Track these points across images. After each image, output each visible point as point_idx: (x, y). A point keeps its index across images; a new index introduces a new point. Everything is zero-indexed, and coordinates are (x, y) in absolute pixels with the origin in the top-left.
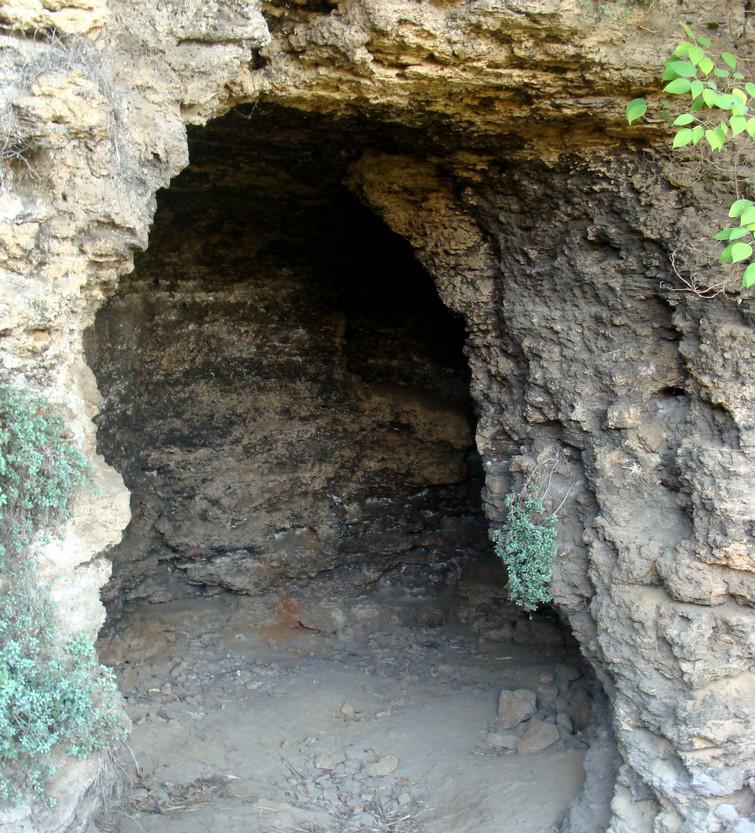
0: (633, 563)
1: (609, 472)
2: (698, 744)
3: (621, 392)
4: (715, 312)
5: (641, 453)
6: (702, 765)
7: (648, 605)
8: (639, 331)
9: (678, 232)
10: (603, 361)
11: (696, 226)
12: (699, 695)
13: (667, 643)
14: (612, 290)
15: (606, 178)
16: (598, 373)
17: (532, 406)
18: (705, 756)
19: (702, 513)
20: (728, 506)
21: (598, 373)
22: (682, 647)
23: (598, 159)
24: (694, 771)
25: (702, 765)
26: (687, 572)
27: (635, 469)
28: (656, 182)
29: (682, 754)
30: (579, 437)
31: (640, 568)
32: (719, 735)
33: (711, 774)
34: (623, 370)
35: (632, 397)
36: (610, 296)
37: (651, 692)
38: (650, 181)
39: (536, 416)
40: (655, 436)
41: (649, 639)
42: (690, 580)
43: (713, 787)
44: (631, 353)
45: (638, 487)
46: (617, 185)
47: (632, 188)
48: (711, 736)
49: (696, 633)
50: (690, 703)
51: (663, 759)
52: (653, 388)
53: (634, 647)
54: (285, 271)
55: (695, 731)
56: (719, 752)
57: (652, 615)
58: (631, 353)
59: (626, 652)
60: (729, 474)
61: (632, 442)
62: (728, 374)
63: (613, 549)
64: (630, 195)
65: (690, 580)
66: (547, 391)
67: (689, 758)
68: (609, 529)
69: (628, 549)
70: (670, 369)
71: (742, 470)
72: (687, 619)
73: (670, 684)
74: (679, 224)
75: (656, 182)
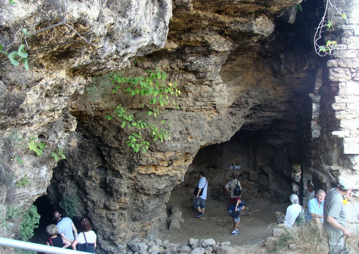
0: (99, 204)
1: (88, 186)
2: (118, 239)
3: (90, 168)
4: (113, 151)
5: (95, 181)
6: (120, 243)
7: (104, 212)
8: (92, 154)
9: (104, 135)
10: (84, 161)
11: (108, 134)
12: (117, 229)
13: (110, 220)
14: (86, 146)
15: (87, 124)
16: (83, 164)
17: (65, 172)
18: (120, 241)
19: (115, 192)
20: (122, 190)
21: (83, 164)
22: (114, 220)
23: (86, 120)
24: (119, 245)
25: (120, 243)
26: (113, 204)
27: (94, 184)
28: (98, 124)
29: (115, 242)
30: (78, 178)
31: (102, 205)
32: (123, 236)
33: (122, 245)
34: (89, 164)
35: (92, 169)
36: (86, 147)
37: (106, 231)
38: (96, 124)
39: (66, 175)
40: (99, 177)
41: (106, 220)
42: (114, 206)
43: (122, 247)
44: (91, 159)
45: (95, 188)
46: (89, 125)
47: (92, 125)
48: (121, 237)
49: (116, 217)
50: (115, 231)
51: (109, 245)
52: (96, 167)
53: (102, 222)
54: (313, 152)
55: (117, 236)
56: (123, 240)
57: (105, 215)
58: (91, 159)
59: (100, 223)
60: (120, 184)
61: (94, 179)
62: (118, 164)
63: (93, 202)
64: (91, 127)
65: (114, 206)
66: (69, 168)
67: (117, 242)
68: (91, 198)
69: (97, 201)
70: (100, 163)
71: (123, 183)
72: (113, 214)
73: (109, 228)
74: (104, 134)
75: (98, 124)
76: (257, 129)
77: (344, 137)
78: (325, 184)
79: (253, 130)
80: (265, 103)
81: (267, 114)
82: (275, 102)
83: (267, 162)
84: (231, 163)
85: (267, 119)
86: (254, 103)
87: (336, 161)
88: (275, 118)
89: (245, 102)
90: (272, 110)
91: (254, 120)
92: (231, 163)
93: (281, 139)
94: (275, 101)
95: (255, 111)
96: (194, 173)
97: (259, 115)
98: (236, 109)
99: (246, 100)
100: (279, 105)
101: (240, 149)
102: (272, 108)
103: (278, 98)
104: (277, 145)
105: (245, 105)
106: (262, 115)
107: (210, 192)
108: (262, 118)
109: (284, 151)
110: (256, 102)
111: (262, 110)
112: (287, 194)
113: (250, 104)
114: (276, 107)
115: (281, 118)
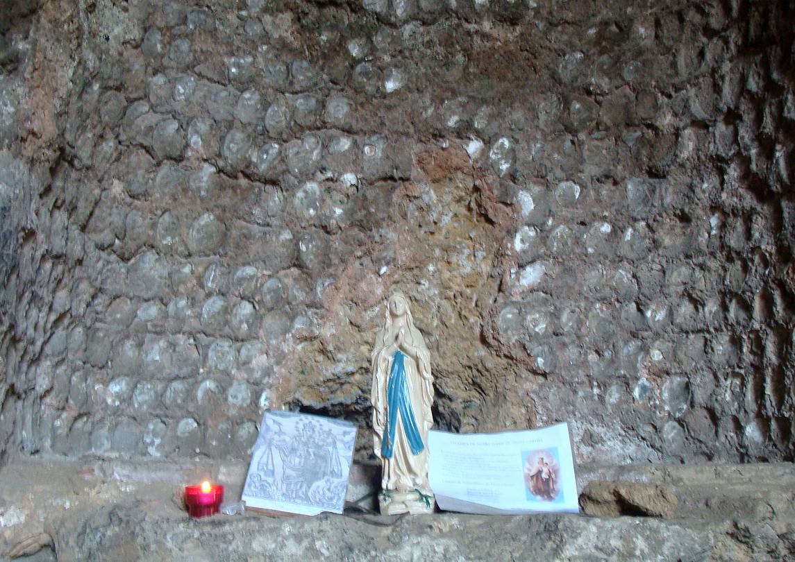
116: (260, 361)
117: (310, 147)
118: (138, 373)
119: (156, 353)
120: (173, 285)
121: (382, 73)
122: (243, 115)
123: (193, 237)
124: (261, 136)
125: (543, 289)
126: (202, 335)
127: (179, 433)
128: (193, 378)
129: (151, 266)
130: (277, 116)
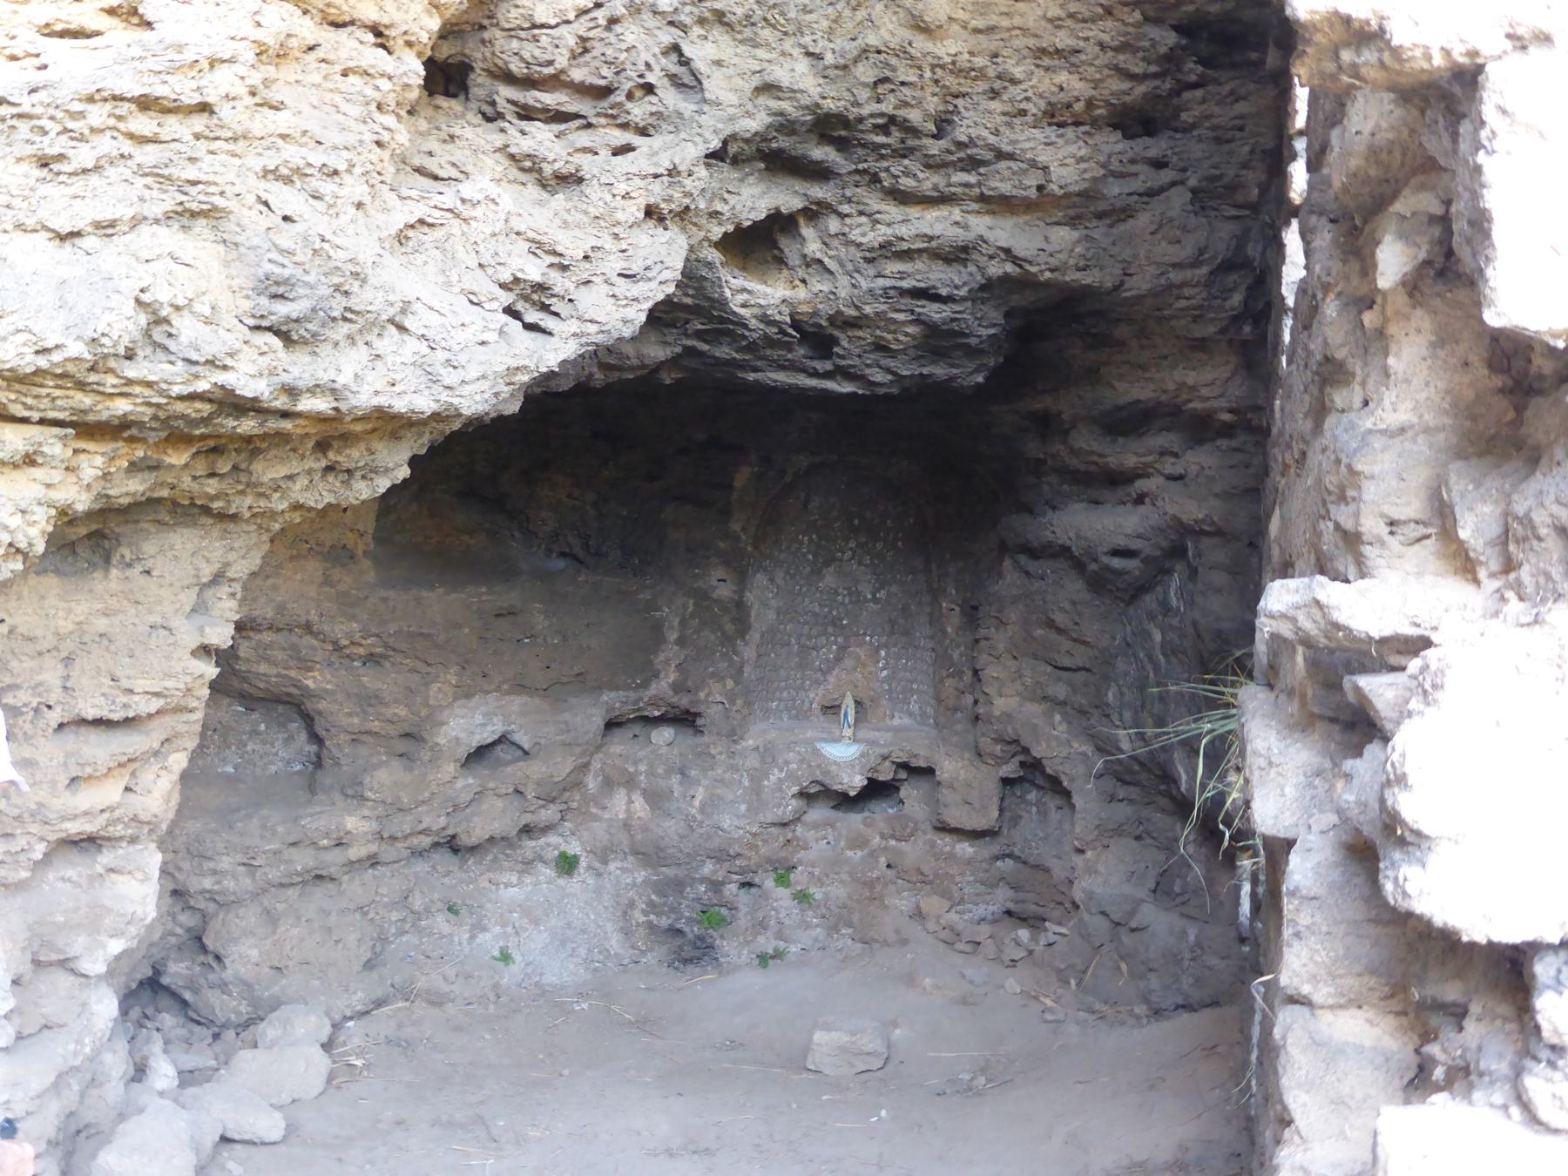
76: (879, 377)
77: (1490, 43)
78: (1279, 849)
79: (846, 388)
80: (887, 107)
81: (937, 223)
82: (995, 105)
83: (1060, 691)
84: (816, 696)
85: (938, 276)
86: (768, 88)
87: (1410, 506)
88: (1010, 268)
89: (671, 64)
90: (971, 178)
91: (821, 285)
92: (816, 696)
93: (1140, 500)
94: (994, 94)
95: (818, 191)
96: (515, 760)
97: (855, 235)
98: (584, 139)
99: (676, 48)
100: (1031, 140)
101: (881, 595)
102: (974, 164)
103: (1018, 72)
104: (1116, 553)
105: (670, 98)
106: (882, 233)
107: (651, 904)
108: (892, 267)
109: (1174, 602)
110: (781, 74)
111: (875, 179)
112: (1198, 944)
113: (716, 86)
114: (1001, 155)
115: (1071, 276)
116: (812, 695)
117: (823, 640)
118: (780, 700)
119: (785, 694)
120: (788, 678)
121: (842, 620)
122: (805, 632)
123: (793, 665)
124: (810, 637)
125: (887, 678)
126: (797, 690)
127: (1347, 682)
128: (794, 700)
129: (783, 673)
130: (814, 632)
